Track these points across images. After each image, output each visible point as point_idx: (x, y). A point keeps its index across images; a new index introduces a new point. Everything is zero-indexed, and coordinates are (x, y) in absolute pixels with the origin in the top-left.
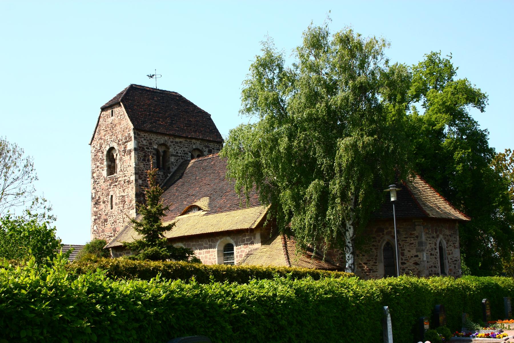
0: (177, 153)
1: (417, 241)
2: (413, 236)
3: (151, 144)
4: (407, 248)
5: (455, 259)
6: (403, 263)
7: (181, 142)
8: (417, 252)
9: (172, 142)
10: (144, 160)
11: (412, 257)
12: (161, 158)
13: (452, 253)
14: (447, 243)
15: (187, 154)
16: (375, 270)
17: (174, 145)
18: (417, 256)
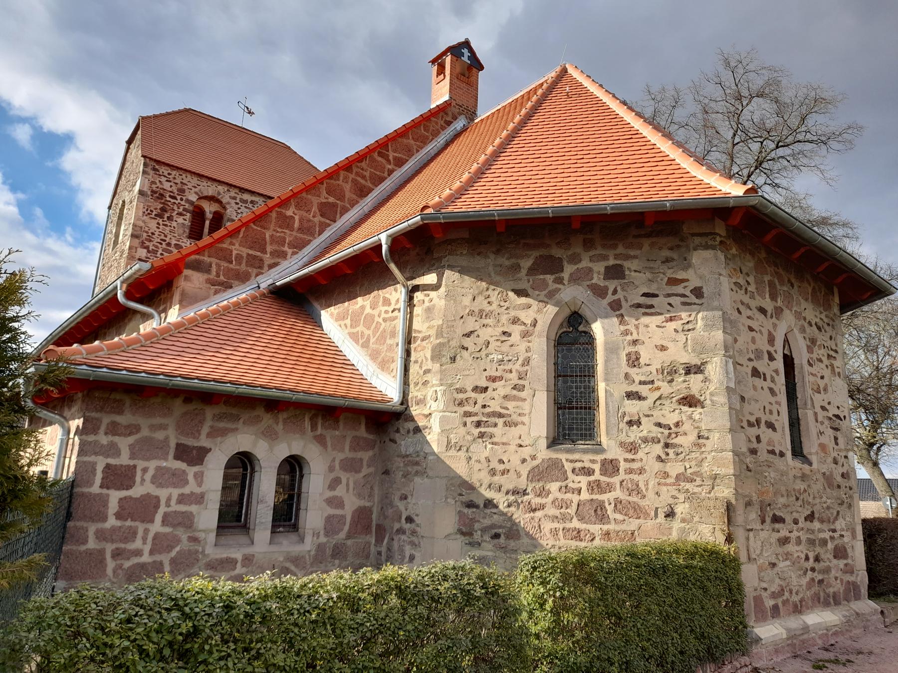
2: (679, 289)
3: (181, 191)
5: (837, 412)
7: (252, 202)
10: (160, 216)
13: (825, 390)
14: (810, 350)
16: (515, 417)
17: (237, 204)
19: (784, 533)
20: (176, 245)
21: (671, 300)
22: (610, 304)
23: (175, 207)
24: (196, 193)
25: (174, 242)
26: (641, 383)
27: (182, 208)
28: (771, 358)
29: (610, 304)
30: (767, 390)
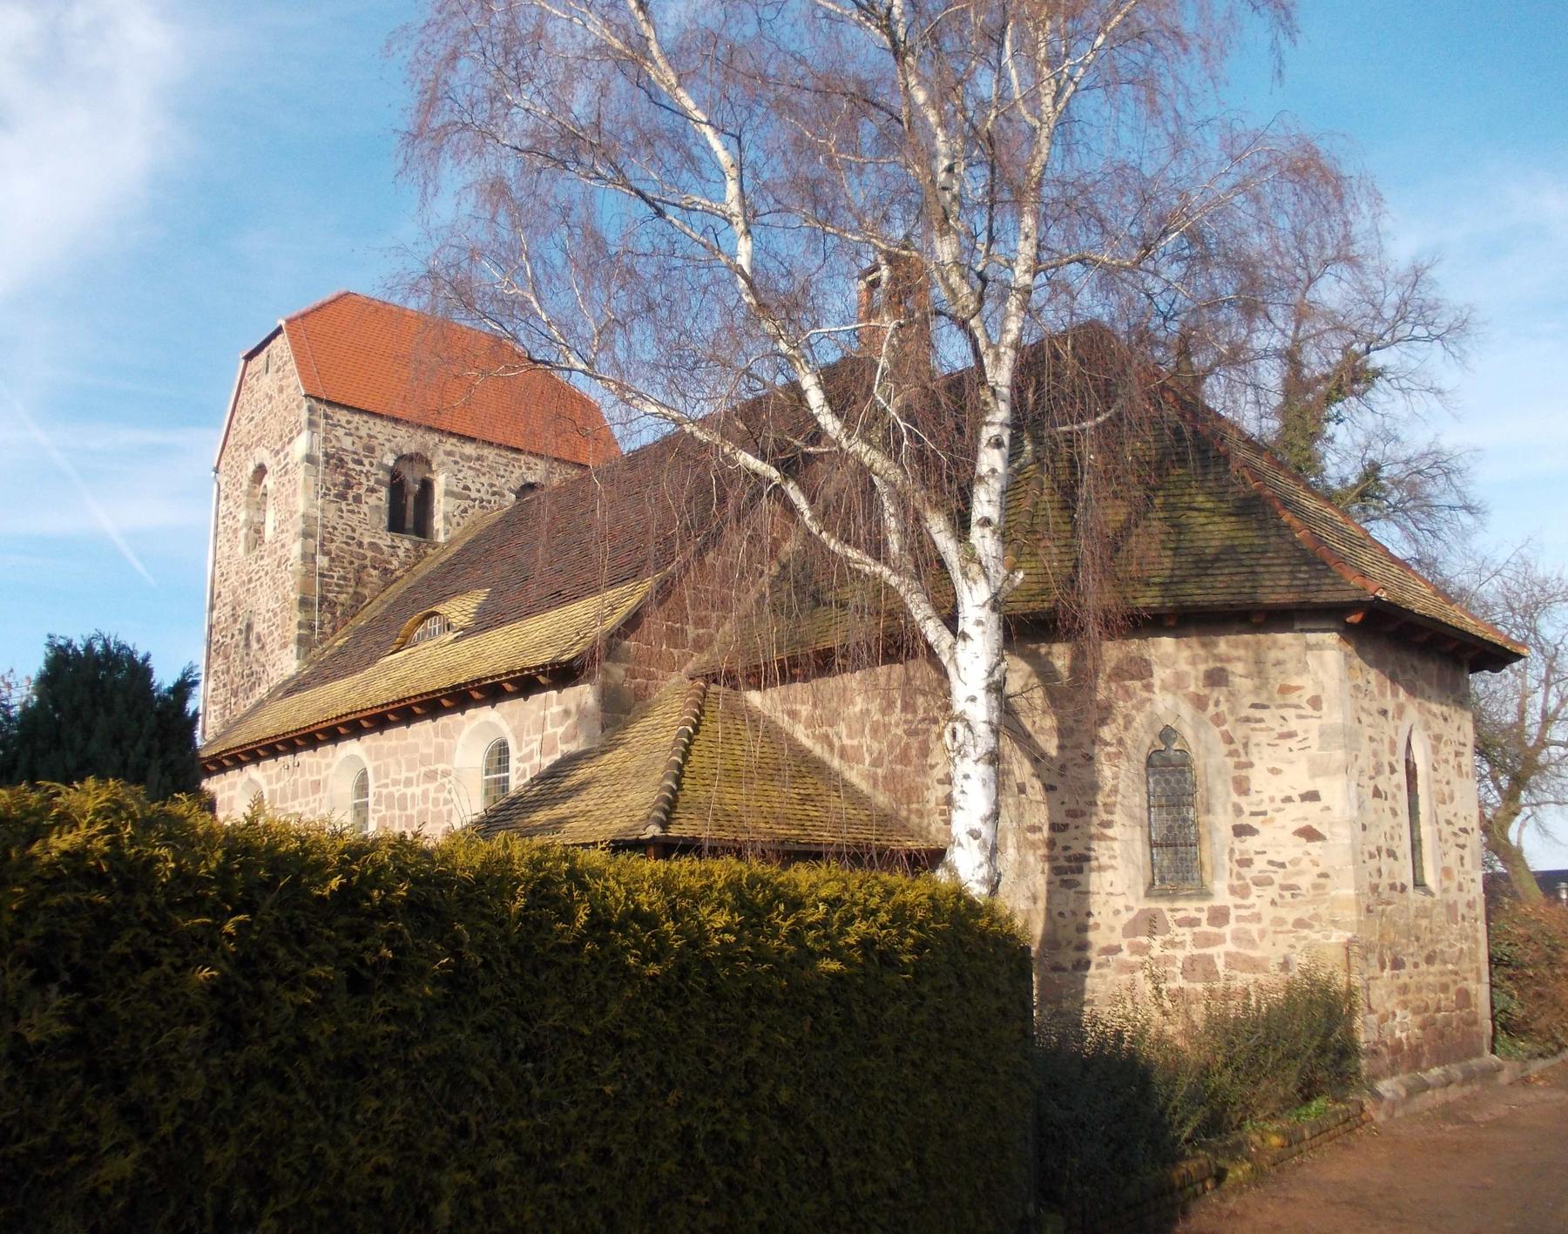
0: (466, 488)
1: (1314, 724)
4: (1262, 759)
6: (1241, 831)
8: (1313, 776)
9: (449, 454)
11: (1288, 799)
12: (411, 499)
13: (1452, 798)
15: (503, 496)
17: (456, 463)
18: (1312, 796)
19: (1404, 979)
20: (371, 544)
21: (1284, 712)
22: (1212, 719)
23: (363, 479)
24: (392, 451)
25: (366, 540)
26: (1253, 814)
27: (372, 479)
28: (1393, 771)
29: (1212, 719)
30: (1388, 812)
